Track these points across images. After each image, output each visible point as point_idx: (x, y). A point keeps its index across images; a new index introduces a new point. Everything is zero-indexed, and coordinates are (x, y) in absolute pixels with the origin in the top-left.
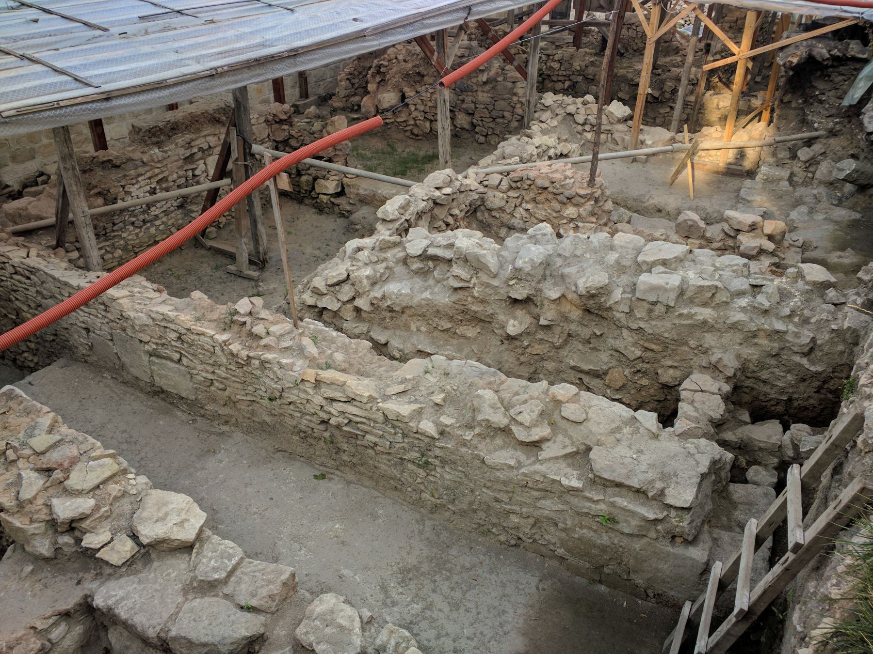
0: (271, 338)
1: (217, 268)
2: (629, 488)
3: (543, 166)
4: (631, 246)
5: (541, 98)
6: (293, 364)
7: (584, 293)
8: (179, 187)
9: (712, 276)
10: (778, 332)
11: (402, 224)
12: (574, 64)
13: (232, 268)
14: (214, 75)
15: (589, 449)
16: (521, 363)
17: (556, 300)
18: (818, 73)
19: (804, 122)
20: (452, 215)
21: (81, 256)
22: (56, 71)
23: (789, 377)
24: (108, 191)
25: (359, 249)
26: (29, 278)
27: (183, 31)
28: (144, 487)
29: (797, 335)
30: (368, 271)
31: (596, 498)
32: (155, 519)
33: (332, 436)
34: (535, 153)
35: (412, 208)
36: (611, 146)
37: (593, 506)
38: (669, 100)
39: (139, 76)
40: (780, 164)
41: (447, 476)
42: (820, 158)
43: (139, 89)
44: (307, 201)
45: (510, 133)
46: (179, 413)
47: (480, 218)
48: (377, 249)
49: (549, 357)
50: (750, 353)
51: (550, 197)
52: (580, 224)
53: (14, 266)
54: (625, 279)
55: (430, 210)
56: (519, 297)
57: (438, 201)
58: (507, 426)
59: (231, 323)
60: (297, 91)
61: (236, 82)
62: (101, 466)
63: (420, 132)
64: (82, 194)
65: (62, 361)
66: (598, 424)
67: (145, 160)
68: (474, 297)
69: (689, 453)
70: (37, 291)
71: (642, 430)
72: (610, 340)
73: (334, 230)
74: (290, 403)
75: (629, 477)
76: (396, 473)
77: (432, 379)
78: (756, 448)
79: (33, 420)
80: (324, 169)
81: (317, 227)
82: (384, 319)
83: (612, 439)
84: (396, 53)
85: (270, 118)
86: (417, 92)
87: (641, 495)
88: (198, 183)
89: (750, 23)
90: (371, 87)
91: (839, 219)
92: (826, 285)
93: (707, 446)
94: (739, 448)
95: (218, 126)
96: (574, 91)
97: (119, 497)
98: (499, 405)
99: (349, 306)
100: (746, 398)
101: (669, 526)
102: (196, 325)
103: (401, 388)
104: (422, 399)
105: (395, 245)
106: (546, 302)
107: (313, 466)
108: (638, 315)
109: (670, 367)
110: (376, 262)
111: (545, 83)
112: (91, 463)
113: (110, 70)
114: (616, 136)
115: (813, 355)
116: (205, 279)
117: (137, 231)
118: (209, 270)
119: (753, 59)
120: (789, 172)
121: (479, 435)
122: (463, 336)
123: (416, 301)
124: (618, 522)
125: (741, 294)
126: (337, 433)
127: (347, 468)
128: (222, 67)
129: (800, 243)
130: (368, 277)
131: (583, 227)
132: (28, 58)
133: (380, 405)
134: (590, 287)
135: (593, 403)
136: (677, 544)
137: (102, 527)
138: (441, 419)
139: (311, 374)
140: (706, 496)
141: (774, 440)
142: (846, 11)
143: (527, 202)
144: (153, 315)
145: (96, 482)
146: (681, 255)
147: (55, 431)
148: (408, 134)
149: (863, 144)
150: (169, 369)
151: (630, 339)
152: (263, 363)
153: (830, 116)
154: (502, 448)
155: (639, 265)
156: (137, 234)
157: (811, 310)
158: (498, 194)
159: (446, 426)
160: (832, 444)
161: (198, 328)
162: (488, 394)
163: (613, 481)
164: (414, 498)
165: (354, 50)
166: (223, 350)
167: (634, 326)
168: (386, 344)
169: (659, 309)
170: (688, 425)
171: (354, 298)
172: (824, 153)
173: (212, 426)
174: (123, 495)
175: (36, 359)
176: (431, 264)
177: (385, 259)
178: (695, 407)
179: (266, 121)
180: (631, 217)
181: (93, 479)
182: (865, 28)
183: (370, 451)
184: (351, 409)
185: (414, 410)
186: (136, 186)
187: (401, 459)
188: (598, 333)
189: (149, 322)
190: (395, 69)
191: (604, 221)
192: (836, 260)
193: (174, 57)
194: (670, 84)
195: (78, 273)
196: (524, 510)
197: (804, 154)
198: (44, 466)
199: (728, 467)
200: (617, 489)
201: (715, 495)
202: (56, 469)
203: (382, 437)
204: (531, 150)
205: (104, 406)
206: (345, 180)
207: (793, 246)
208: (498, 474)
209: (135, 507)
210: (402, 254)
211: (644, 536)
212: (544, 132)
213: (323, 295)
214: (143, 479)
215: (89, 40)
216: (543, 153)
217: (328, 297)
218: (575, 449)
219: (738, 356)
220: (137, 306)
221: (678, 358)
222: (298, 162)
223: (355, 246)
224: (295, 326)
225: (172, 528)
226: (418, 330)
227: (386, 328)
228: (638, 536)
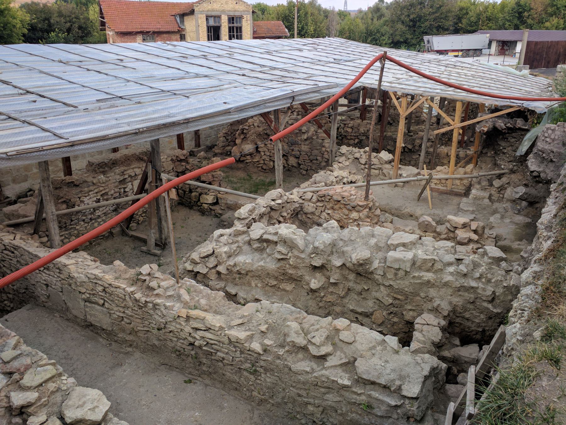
0: (161, 289)
1: (134, 249)
2: (379, 384)
3: (338, 188)
4: (385, 235)
5: (339, 149)
6: (173, 306)
7: (356, 262)
8: (115, 198)
9: (433, 253)
10: (473, 288)
11: (250, 221)
12: (361, 129)
13: (144, 248)
14: (137, 133)
15: (355, 360)
16: (320, 308)
17: (340, 267)
18: (501, 137)
19: (496, 165)
20: (282, 216)
21: (49, 240)
22: (43, 130)
23: (482, 316)
24: (70, 200)
25: (222, 235)
26: (13, 253)
27: (122, 108)
28: (72, 385)
29: (484, 290)
30: (226, 249)
31: (359, 392)
32: (76, 406)
33: (196, 354)
34: (334, 180)
35: (256, 212)
36: (382, 177)
37: (358, 397)
38: (418, 151)
39: (92, 133)
40: (484, 189)
41: (268, 380)
42: (506, 185)
43: (91, 140)
44: (195, 208)
45: (321, 169)
46: (101, 340)
47: (300, 218)
48: (232, 235)
49: (337, 303)
50: (458, 301)
51: (342, 206)
52: (361, 223)
53: (4, 245)
54: (380, 255)
55: (268, 213)
56: (317, 265)
57: (273, 207)
58: (305, 346)
59: (137, 280)
60: (193, 143)
61: (151, 137)
62: (45, 371)
63: (267, 168)
64: (52, 201)
65: (28, 306)
66: (362, 344)
67: (94, 182)
68: (290, 265)
69: (417, 363)
70: (18, 261)
71: (388, 348)
72: (373, 293)
73: (210, 225)
74: (171, 332)
75: (379, 378)
76: (236, 378)
77: (260, 316)
78: (463, 362)
79: (4, 341)
80: (207, 188)
81: (200, 223)
82: (235, 279)
83: (369, 353)
84: (253, 122)
85: (174, 158)
86: (265, 145)
87: (387, 390)
88: (127, 196)
89: (459, 107)
90: (238, 141)
91: (519, 222)
92: (500, 259)
93: (429, 358)
94: (453, 362)
95: (142, 162)
96: (360, 145)
97: (54, 392)
98: (301, 332)
99: (213, 270)
100: (457, 330)
101: (405, 410)
102: (115, 282)
103: (240, 321)
104: (253, 328)
105: (244, 233)
106: (333, 268)
107: (184, 374)
108: (389, 277)
109: (411, 310)
110: (232, 243)
111: (342, 140)
112: (39, 369)
113: (81, 128)
114: (385, 171)
115: (494, 302)
116: (127, 255)
117: (86, 225)
118: (129, 250)
119: (463, 128)
120: (488, 194)
121: (288, 351)
122: (284, 290)
123: (255, 267)
124: (374, 408)
125: (450, 264)
126: (199, 351)
127: (206, 376)
128: (142, 128)
129: (494, 236)
130: (225, 252)
131: (363, 225)
132: (27, 122)
133: (226, 332)
134: (359, 259)
135: (359, 331)
136: (411, 423)
137: (41, 412)
138: (265, 341)
139: (184, 313)
140: (429, 391)
141: (474, 356)
142: (513, 103)
143: (328, 209)
144: (89, 276)
145: (41, 381)
146: (414, 241)
147: (18, 348)
148: (260, 169)
149: (529, 178)
150: (96, 310)
151: (385, 292)
152: (155, 305)
153: (510, 161)
154: (302, 360)
155: (389, 246)
156: (86, 227)
157: (492, 274)
158: (310, 204)
159: (268, 346)
160: (490, 351)
161: (116, 283)
162: (294, 325)
163: (369, 381)
164: (248, 395)
165: (223, 120)
166: (130, 298)
167: (387, 284)
168: (236, 295)
169: (401, 273)
170: (418, 345)
171: (216, 266)
172: (509, 183)
173: (121, 348)
174: (57, 391)
175: (12, 305)
176: (265, 244)
177: (237, 242)
178: (423, 334)
179: (172, 160)
180: (392, 219)
181: (38, 380)
182: (525, 112)
183: (220, 364)
184: (208, 335)
185: (248, 336)
186: (88, 198)
187: (239, 368)
188: (366, 288)
189: (86, 280)
190: (252, 131)
191: (376, 221)
192: (517, 246)
193: (114, 122)
194: (418, 142)
195: (45, 249)
196: (316, 402)
197: (497, 183)
198: (8, 371)
199: (443, 373)
200: (372, 386)
201: (436, 391)
202: (15, 373)
203: (227, 353)
204: (332, 178)
205: (53, 335)
206: (219, 195)
207: (490, 237)
208: (300, 377)
209: (65, 398)
210: (247, 238)
211: (390, 417)
212: (340, 168)
213: (197, 263)
214: (72, 380)
215: (65, 113)
216: (340, 181)
217: (200, 265)
218: (347, 361)
219: (450, 303)
220: (80, 270)
221: (414, 304)
222: (184, 182)
223: (219, 233)
224: (178, 282)
225: (87, 412)
226: (256, 286)
227: (236, 285)
228: (386, 417)
